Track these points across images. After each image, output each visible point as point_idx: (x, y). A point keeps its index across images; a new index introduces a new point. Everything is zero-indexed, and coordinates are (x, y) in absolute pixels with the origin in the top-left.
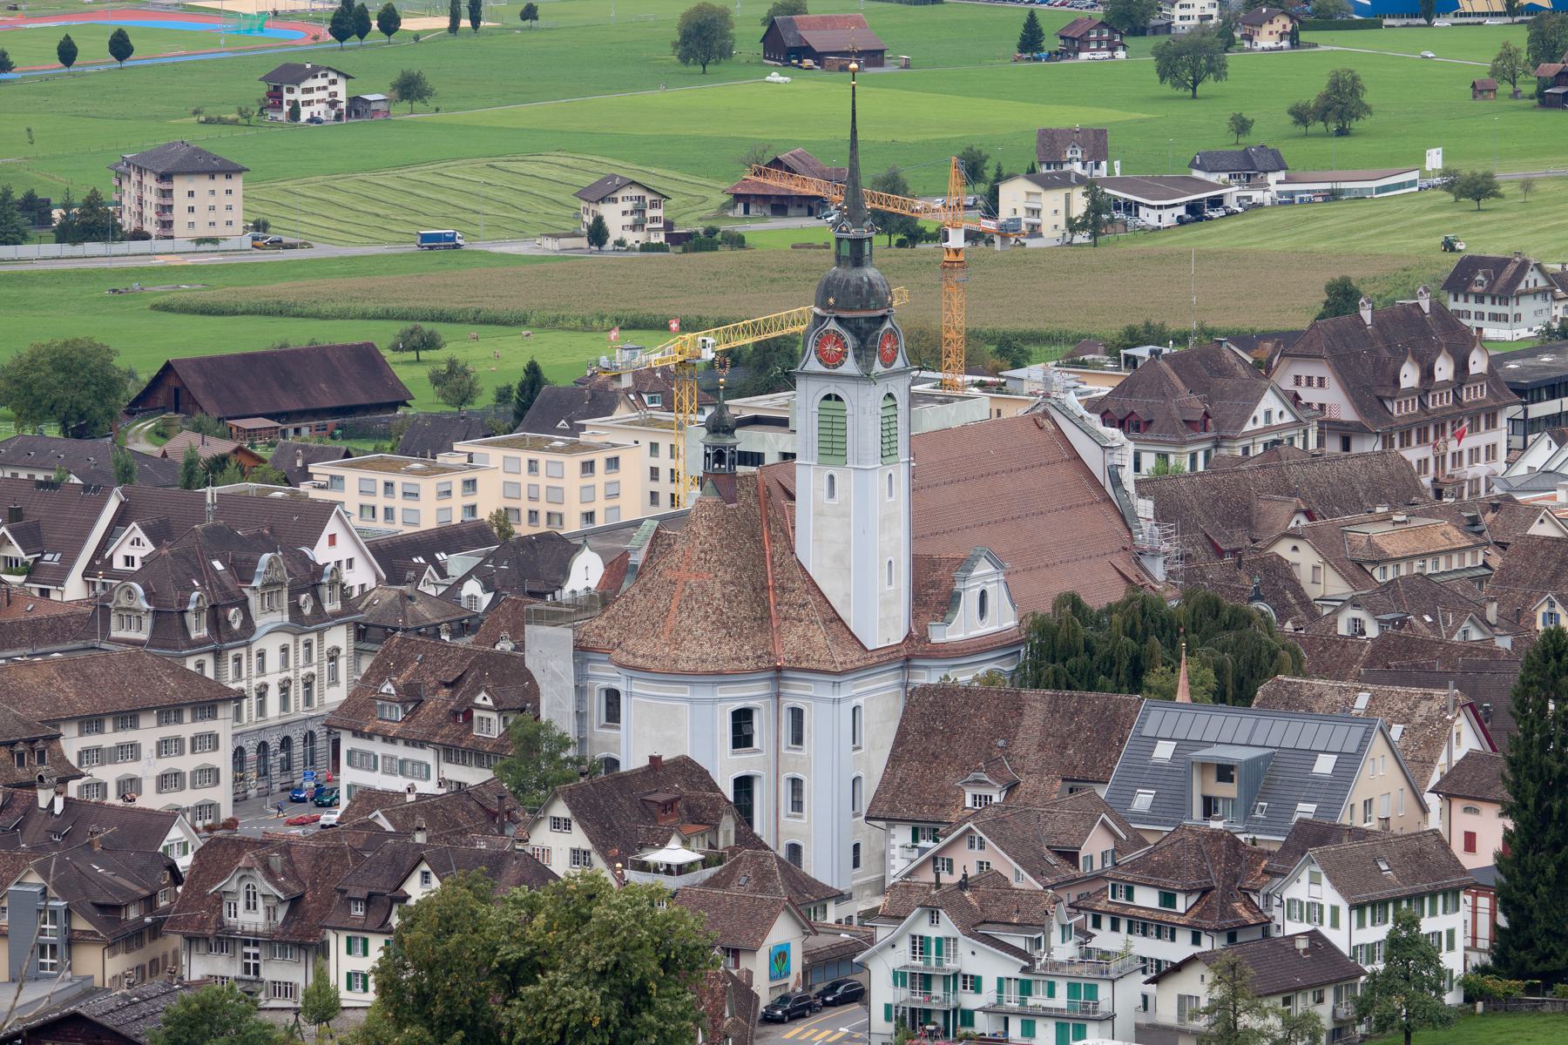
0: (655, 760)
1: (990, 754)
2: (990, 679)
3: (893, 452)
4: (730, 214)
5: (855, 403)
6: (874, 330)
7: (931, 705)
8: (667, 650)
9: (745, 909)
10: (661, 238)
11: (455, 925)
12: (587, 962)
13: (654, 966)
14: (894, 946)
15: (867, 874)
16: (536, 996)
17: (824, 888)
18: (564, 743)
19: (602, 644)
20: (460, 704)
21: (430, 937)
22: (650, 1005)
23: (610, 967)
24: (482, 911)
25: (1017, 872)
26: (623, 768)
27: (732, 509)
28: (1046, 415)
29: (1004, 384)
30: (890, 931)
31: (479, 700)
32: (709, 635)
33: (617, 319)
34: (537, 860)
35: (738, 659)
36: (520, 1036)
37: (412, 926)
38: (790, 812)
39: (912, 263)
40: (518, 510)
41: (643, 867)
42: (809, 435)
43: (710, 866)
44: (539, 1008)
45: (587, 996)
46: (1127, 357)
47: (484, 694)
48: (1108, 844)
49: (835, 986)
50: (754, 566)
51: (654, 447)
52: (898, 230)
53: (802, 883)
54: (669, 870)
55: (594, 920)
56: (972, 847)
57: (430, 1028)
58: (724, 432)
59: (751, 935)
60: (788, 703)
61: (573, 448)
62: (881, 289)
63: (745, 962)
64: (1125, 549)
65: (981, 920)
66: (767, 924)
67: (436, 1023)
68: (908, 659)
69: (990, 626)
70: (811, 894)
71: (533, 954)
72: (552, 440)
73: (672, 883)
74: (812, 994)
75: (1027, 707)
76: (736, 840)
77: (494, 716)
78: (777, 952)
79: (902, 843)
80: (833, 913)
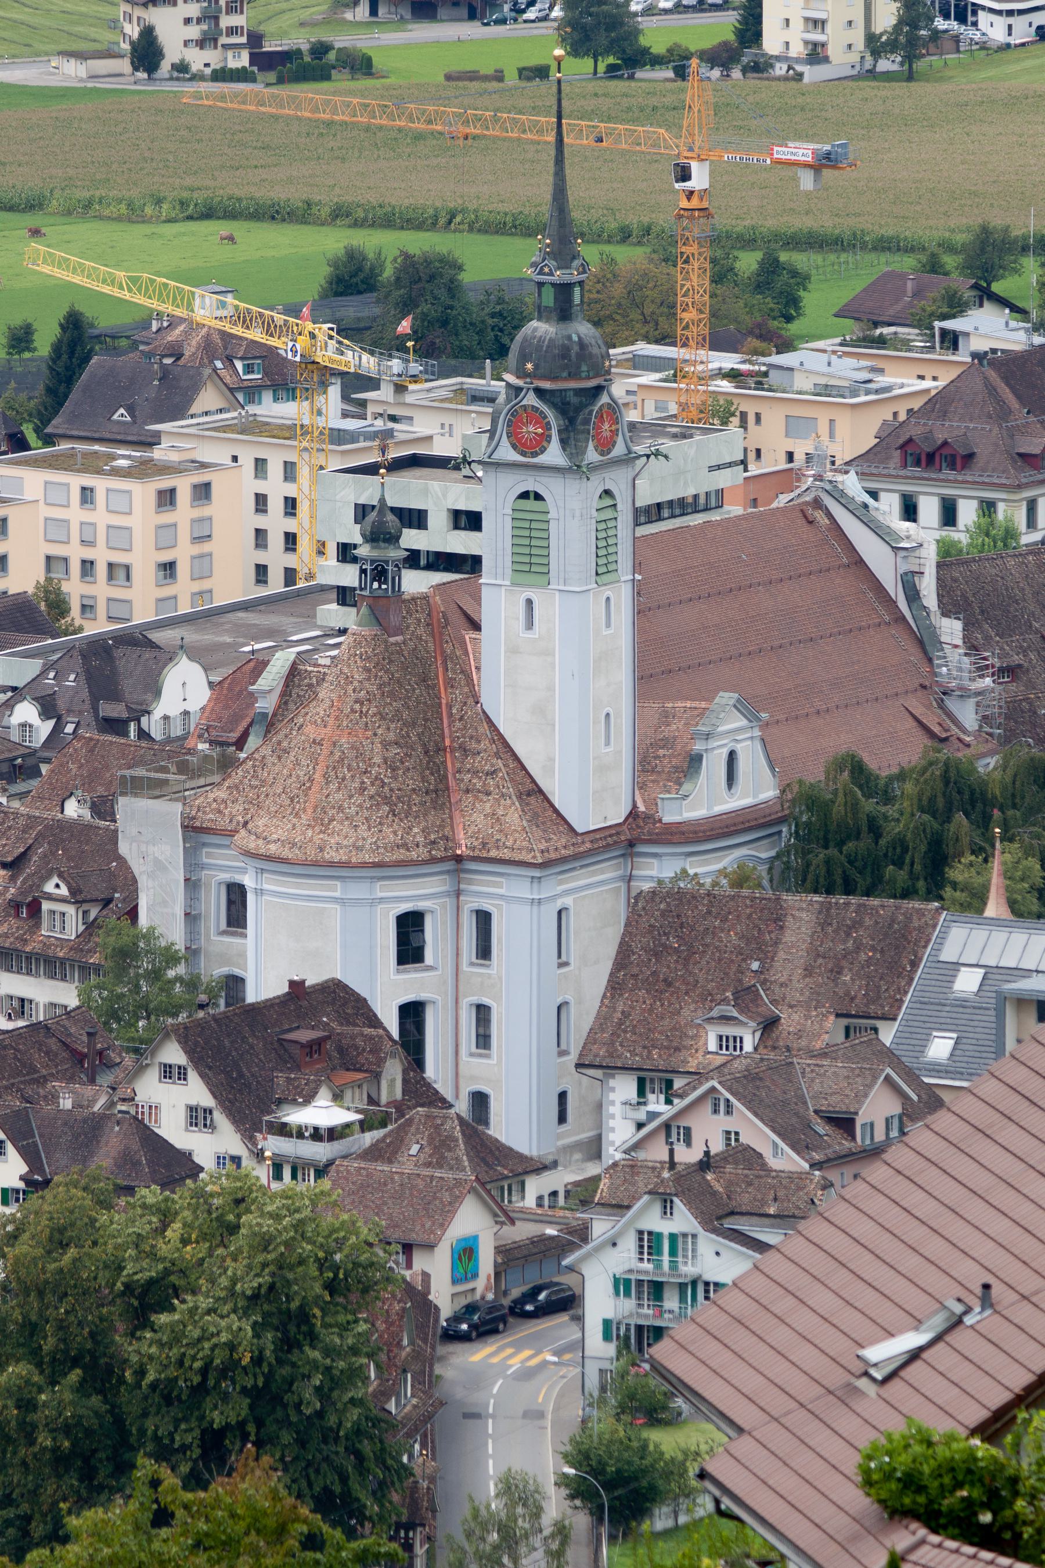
0: (296, 986)
1: (740, 981)
2: (741, 879)
3: (611, 567)
4: (349, 16)
5: (561, 504)
6: (586, 406)
7: (663, 915)
8: (310, 833)
9: (420, 1191)
10: (242, 60)
11: (71, 1238)
12: (235, 1284)
13: (318, 1289)
14: (614, 1244)
15: (576, 1131)
16: (172, 1325)
17: (521, 1157)
18: (171, 958)
19: (223, 823)
20: (22, 893)
21: (39, 1252)
22: (313, 1337)
23: (263, 1291)
24: (103, 1218)
25: (775, 1145)
26: (252, 996)
27: (396, 644)
28: (817, 503)
29: (766, 374)
30: (609, 1225)
31: (49, 887)
32: (366, 814)
33: (182, 203)
34: (142, 1122)
35: (405, 846)
36: (151, 1376)
37: (16, 1237)
38: (474, 1049)
39: (629, 109)
40: (66, 560)
41: (283, 1130)
42: (500, 545)
43: (371, 1128)
44: (175, 1340)
45: (235, 1328)
46: (944, 333)
47: (56, 880)
48: (894, 1108)
49: (537, 1290)
50: (426, 720)
51: (260, 465)
52: (607, 52)
53: (491, 1152)
54: (317, 1135)
55: (243, 1231)
56: (716, 1111)
57: (39, 1365)
58: (385, 541)
59: (428, 1225)
60: (471, 904)
61: (143, 470)
62: (595, 351)
63: (420, 1262)
64: (923, 687)
65: (727, 1210)
66: (448, 1212)
67: (47, 1359)
68: (631, 844)
69: (739, 799)
70: (505, 1167)
71: (167, 1272)
72: (114, 457)
73: (320, 1151)
74: (506, 1302)
75: (790, 918)
76: (404, 1092)
77: (70, 910)
78: (463, 1245)
79: (623, 1099)
80: (535, 1187)
